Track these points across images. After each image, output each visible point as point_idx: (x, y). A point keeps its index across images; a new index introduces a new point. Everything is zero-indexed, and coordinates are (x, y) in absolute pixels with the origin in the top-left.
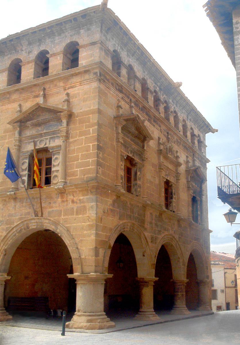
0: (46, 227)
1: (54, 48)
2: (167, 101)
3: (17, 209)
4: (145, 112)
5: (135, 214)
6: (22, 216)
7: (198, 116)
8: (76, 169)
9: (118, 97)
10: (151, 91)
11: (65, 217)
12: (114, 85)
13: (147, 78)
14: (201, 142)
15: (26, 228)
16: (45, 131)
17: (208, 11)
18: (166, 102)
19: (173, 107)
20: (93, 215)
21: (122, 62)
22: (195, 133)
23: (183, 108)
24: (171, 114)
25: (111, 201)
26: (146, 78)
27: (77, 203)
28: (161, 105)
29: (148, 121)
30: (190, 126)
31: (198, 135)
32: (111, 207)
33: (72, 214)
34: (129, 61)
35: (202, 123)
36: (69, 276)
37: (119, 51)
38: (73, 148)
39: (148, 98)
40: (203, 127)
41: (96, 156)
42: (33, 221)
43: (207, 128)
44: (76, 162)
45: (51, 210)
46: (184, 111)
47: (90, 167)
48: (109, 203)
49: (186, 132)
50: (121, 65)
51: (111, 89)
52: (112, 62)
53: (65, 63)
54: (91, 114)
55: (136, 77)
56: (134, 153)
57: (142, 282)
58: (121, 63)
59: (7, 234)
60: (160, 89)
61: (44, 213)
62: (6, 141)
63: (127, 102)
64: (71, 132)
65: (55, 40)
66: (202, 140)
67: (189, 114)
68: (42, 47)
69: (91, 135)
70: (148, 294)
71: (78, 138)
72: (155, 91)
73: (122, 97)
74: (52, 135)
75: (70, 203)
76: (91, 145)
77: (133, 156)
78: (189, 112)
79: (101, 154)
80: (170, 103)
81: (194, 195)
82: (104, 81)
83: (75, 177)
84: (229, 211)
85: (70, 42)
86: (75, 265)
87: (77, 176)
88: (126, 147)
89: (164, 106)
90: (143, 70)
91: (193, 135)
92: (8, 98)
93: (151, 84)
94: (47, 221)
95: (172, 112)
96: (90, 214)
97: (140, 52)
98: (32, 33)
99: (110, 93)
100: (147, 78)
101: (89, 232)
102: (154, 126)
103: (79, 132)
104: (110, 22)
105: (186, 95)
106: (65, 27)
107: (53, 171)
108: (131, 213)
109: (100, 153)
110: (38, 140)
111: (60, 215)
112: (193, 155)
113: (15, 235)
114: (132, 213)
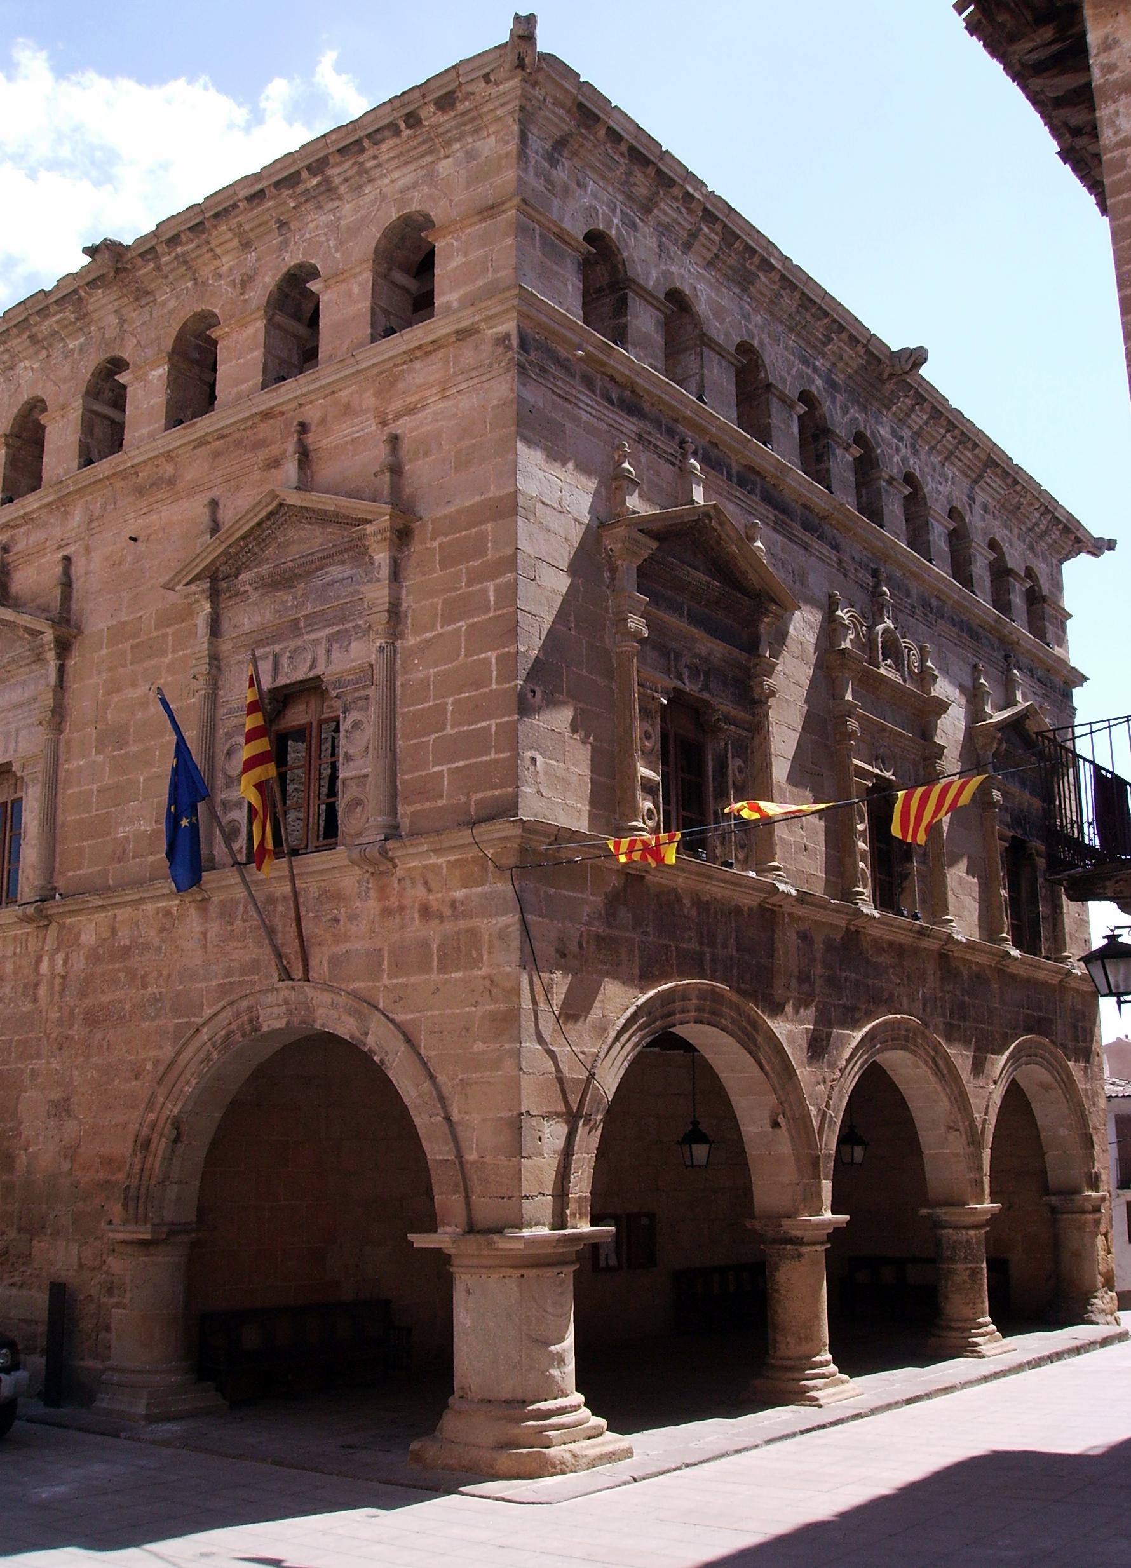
0: (322, 1026)
1: (337, 251)
2: (868, 433)
3: (209, 946)
4: (758, 491)
5: (725, 946)
6: (233, 979)
7: (1018, 488)
8: (437, 769)
9: (616, 436)
10: (783, 399)
11: (395, 981)
12: (599, 384)
13: (761, 343)
14: (1044, 599)
15: (248, 1028)
16: (309, 609)
17: (972, 8)
18: (860, 438)
19: (896, 459)
20: (509, 969)
21: (634, 282)
22: (1010, 565)
23: (947, 458)
24: (888, 488)
25: (598, 900)
26: (756, 343)
27: (441, 917)
28: (839, 451)
29: (774, 529)
30: (985, 533)
31: (1029, 570)
32: (599, 928)
33: (424, 966)
34: (667, 274)
35: (1042, 515)
36: (420, 1241)
37: (613, 233)
38: (420, 675)
39: (768, 426)
40: (1046, 532)
41: (514, 705)
42: (271, 998)
43: (1072, 538)
44: (433, 736)
45: (342, 948)
46: (950, 471)
47: (493, 756)
48: (587, 910)
49: (969, 562)
50: (631, 295)
51: (582, 401)
52: (581, 285)
53: (385, 311)
54: (487, 521)
55: (705, 340)
56: (707, 675)
57: (775, 1241)
58: (629, 287)
59: (178, 1054)
60: (832, 385)
61: (313, 962)
62: (167, 660)
63: (665, 452)
64: (408, 602)
65: (339, 219)
66: (1045, 592)
67: (975, 482)
68: (292, 252)
69: (491, 614)
70: (807, 1297)
71: (440, 631)
72: (806, 397)
73: (640, 436)
74: (337, 624)
75: (413, 919)
76: (492, 655)
77: (705, 688)
78: (974, 476)
79: (539, 694)
80: (883, 440)
81: (1019, 833)
82: (543, 370)
83: (433, 805)
84: (1106, 941)
85: (399, 218)
86: (441, 1194)
87: (441, 797)
88: (669, 653)
89: (852, 455)
90: (742, 308)
91: (1000, 572)
92: (171, 482)
93: (782, 364)
94: (327, 997)
95: (891, 481)
96: (499, 966)
97: (716, 234)
98: (250, 199)
99: (577, 420)
100: (761, 343)
101: (492, 1046)
102: (806, 548)
103: (445, 602)
104: (561, 112)
105: (954, 404)
106: (375, 157)
107: (345, 780)
108: (701, 944)
109: (533, 691)
110: (283, 650)
111: (374, 973)
112: (1007, 657)
113: (208, 1057)
114: (708, 945)
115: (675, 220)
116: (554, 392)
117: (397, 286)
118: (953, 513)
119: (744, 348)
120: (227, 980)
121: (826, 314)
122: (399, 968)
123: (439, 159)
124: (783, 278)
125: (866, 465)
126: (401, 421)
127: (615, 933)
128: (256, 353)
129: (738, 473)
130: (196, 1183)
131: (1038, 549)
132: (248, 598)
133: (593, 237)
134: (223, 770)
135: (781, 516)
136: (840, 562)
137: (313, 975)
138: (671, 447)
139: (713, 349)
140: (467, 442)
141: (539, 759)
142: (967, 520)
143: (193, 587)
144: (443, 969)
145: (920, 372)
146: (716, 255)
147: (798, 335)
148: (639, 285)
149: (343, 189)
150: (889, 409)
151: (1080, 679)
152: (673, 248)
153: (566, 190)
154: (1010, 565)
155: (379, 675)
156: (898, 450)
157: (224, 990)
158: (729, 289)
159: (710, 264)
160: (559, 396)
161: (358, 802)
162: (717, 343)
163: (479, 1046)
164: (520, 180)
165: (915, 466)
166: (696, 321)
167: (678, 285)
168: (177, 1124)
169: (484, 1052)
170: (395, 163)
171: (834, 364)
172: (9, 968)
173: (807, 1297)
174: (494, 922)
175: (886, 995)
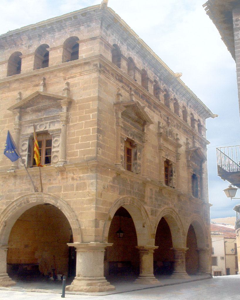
2: (167, 89)
3: (16, 185)
5: (136, 190)
11: (65, 192)
14: (202, 126)
16: (45, 116)
18: (166, 90)
19: (173, 95)
20: (93, 190)
26: (146, 69)
27: (77, 180)
28: (161, 93)
30: (190, 111)
31: (198, 120)
32: (111, 184)
33: (72, 189)
34: (129, 54)
37: (119, 45)
38: (73, 131)
41: (96, 138)
42: (33, 196)
44: (76, 144)
47: (90, 148)
48: (109, 180)
50: (121, 58)
54: (90, 101)
55: (136, 68)
56: (134, 136)
59: (7, 207)
60: (160, 79)
61: (44, 189)
62: (6, 125)
67: (189, 101)
70: (148, 262)
72: (155, 81)
73: (122, 87)
74: (52, 120)
75: (70, 180)
76: (91, 128)
77: (133, 138)
79: (101, 137)
81: (194, 173)
82: (104, 72)
87: (77, 156)
88: (126, 131)
90: (143, 62)
91: (193, 120)
93: (151, 74)
99: (110, 82)
100: (147, 70)
102: (154, 112)
106: (65, 24)
107: (53, 152)
108: (131, 189)
109: (100, 136)
112: (193, 137)
114: (132, 189)
116: (106, 76)
117: (68, 51)
118: (184, 107)
119: (144, 70)
120: (21, 192)
122: (66, 190)
123: (81, 26)
125: (167, 96)
126: (70, 79)
127: (114, 185)
128: (32, 62)
129: (141, 96)
130: (8, 235)
131: (201, 116)
132: (29, 113)
133: (115, 45)
134: (21, 149)
135: (149, 105)
136: (161, 115)
137: (43, 191)
138: (128, 89)
139: (137, 70)
140: (86, 85)
141: (101, 150)
142: (186, 108)
143: (15, 110)
144: (77, 190)
146: (139, 51)
148: (123, 56)
149: (56, 30)
150: (172, 84)
151: (208, 143)
152: (130, 49)
153: (110, 35)
154: (195, 118)
155: (63, 131)
156: (173, 93)
157: (20, 194)
158: (141, 58)
160: (107, 77)
161: (56, 156)
162: (138, 68)
163: (85, 206)
164: (101, 33)
165: (177, 97)
166: (134, 64)
167: (131, 56)
168: (6, 222)
169: (86, 207)
170: (69, 26)
171: (161, 75)
173: (148, 262)
174: (90, 181)
175: (167, 203)
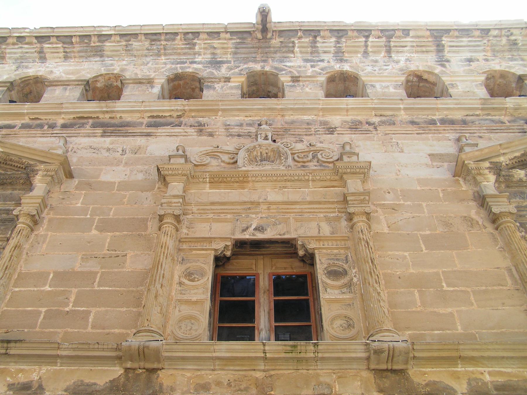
105: (125, 25)
115: (22, 53)
121: (176, 34)
124: (122, 36)
145: (274, 20)
147: (165, 55)
159: (66, 58)
172: (407, 394)
